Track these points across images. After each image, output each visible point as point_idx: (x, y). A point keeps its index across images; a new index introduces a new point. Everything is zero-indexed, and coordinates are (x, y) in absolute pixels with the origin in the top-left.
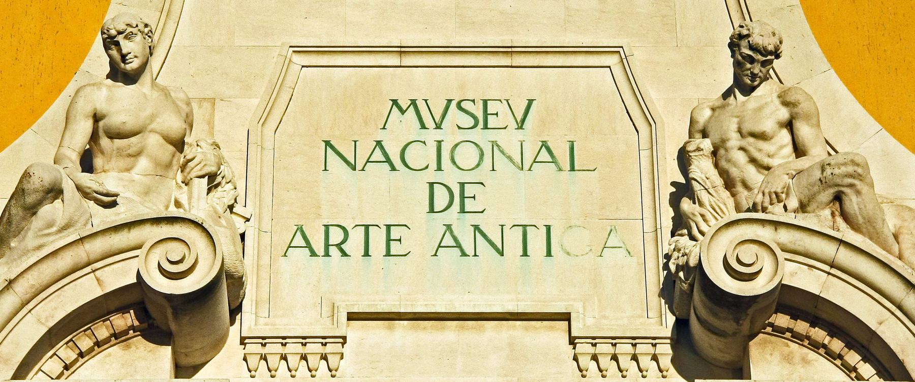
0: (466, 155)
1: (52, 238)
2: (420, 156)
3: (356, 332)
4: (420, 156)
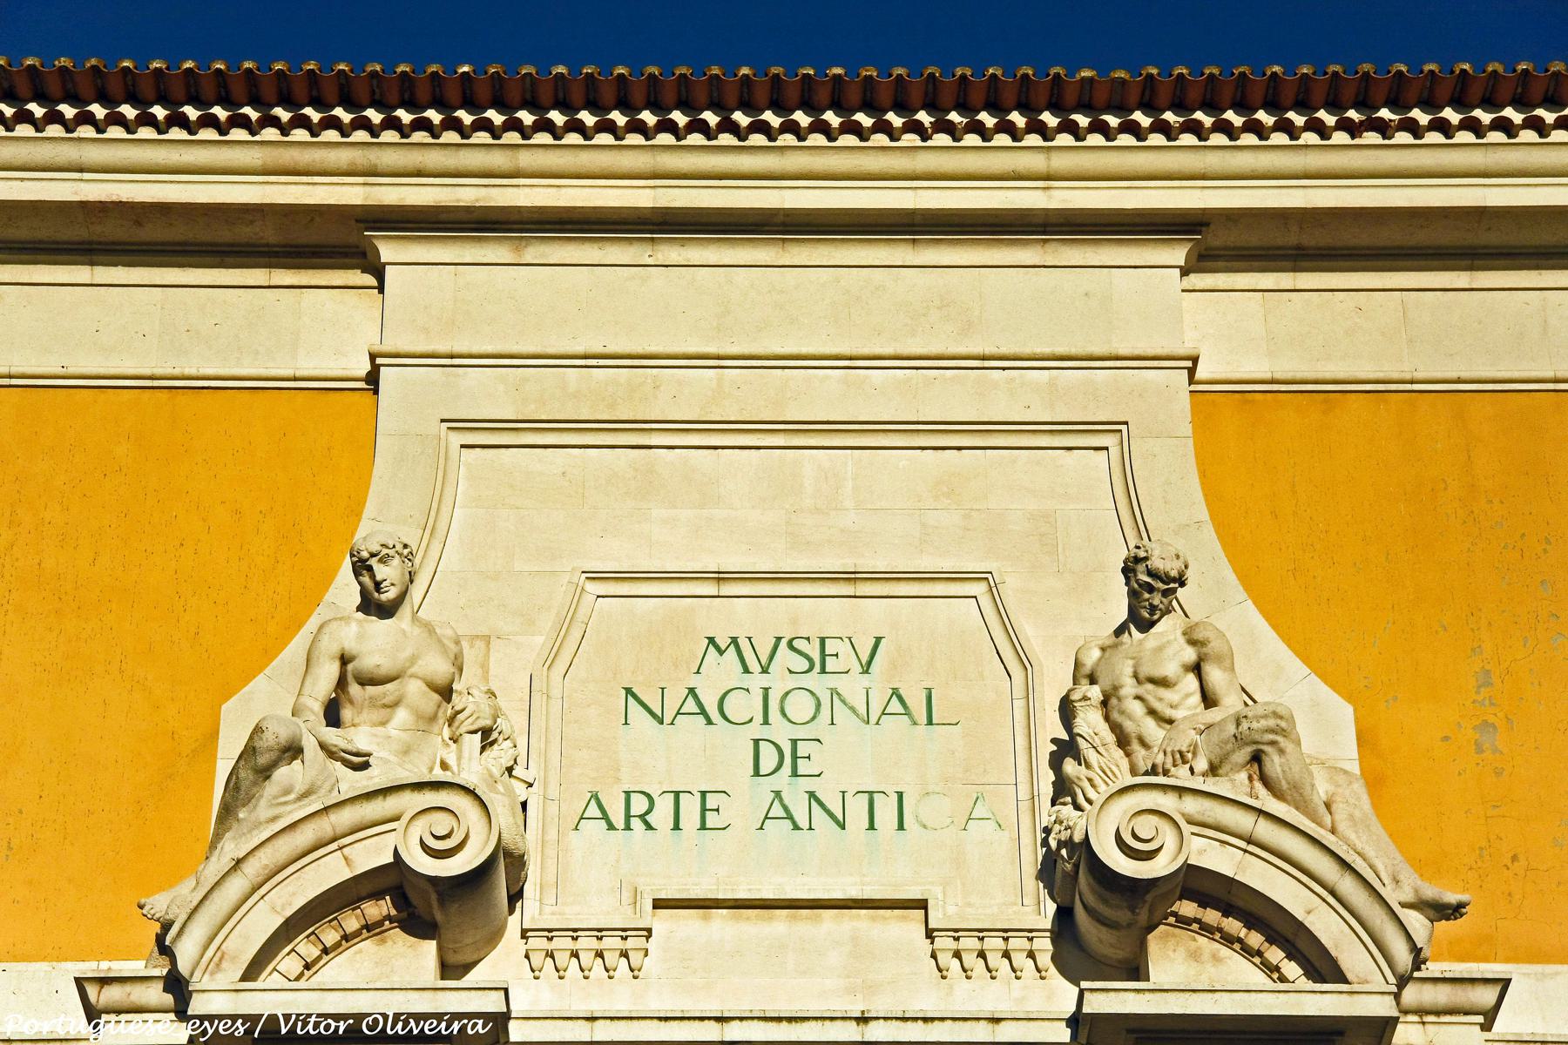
0: (800, 707)
1: (289, 808)
2: (738, 706)
3: (662, 922)
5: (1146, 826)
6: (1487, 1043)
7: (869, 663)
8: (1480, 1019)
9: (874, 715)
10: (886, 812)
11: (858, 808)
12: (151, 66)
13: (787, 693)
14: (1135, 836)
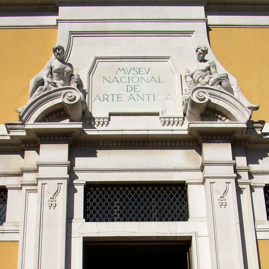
0: (135, 80)
4: (126, 80)
5: (201, 94)
10: (152, 97)
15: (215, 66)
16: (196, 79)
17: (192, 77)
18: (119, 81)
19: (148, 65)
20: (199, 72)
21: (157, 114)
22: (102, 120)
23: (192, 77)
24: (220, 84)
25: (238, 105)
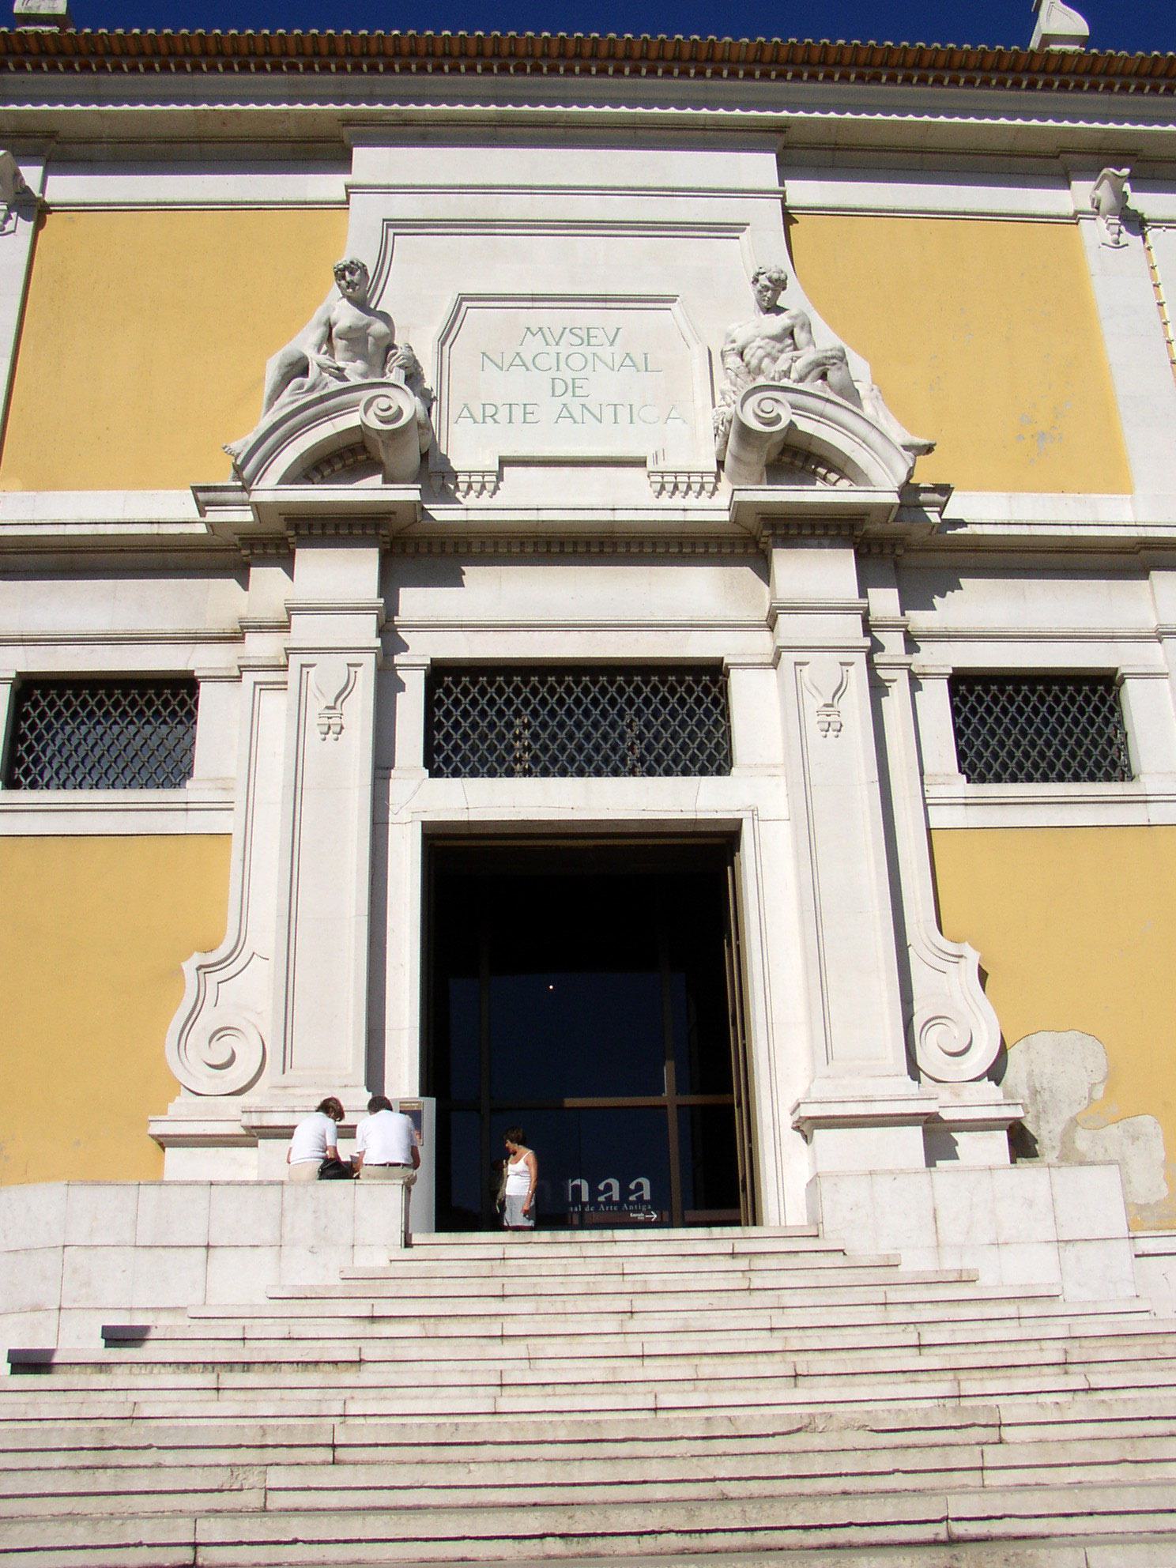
0: (577, 362)
5: (767, 405)
6: (1138, 1259)
7: (613, 341)
8: (938, 509)
9: (616, 368)
10: (624, 414)
11: (608, 412)
12: (790, 40)
13: (569, 356)
14: (763, 411)
15: (807, 326)
16: (754, 362)
17: (741, 355)
18: (531, 367)
19: (614, 318)
20: (762, 343)
21: (641, 463)
22: (480, 479)
23: (741, 355)
24: (823, 376)
25: (873, 437)
